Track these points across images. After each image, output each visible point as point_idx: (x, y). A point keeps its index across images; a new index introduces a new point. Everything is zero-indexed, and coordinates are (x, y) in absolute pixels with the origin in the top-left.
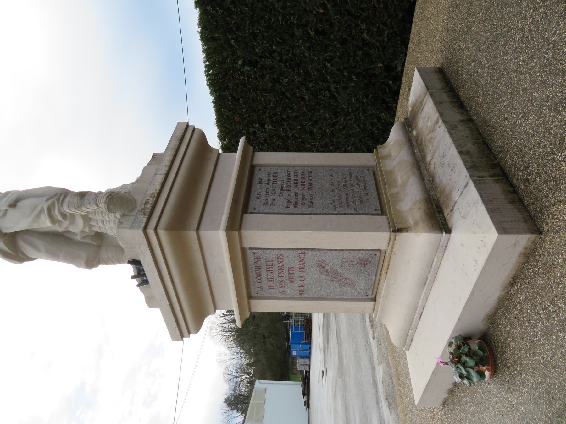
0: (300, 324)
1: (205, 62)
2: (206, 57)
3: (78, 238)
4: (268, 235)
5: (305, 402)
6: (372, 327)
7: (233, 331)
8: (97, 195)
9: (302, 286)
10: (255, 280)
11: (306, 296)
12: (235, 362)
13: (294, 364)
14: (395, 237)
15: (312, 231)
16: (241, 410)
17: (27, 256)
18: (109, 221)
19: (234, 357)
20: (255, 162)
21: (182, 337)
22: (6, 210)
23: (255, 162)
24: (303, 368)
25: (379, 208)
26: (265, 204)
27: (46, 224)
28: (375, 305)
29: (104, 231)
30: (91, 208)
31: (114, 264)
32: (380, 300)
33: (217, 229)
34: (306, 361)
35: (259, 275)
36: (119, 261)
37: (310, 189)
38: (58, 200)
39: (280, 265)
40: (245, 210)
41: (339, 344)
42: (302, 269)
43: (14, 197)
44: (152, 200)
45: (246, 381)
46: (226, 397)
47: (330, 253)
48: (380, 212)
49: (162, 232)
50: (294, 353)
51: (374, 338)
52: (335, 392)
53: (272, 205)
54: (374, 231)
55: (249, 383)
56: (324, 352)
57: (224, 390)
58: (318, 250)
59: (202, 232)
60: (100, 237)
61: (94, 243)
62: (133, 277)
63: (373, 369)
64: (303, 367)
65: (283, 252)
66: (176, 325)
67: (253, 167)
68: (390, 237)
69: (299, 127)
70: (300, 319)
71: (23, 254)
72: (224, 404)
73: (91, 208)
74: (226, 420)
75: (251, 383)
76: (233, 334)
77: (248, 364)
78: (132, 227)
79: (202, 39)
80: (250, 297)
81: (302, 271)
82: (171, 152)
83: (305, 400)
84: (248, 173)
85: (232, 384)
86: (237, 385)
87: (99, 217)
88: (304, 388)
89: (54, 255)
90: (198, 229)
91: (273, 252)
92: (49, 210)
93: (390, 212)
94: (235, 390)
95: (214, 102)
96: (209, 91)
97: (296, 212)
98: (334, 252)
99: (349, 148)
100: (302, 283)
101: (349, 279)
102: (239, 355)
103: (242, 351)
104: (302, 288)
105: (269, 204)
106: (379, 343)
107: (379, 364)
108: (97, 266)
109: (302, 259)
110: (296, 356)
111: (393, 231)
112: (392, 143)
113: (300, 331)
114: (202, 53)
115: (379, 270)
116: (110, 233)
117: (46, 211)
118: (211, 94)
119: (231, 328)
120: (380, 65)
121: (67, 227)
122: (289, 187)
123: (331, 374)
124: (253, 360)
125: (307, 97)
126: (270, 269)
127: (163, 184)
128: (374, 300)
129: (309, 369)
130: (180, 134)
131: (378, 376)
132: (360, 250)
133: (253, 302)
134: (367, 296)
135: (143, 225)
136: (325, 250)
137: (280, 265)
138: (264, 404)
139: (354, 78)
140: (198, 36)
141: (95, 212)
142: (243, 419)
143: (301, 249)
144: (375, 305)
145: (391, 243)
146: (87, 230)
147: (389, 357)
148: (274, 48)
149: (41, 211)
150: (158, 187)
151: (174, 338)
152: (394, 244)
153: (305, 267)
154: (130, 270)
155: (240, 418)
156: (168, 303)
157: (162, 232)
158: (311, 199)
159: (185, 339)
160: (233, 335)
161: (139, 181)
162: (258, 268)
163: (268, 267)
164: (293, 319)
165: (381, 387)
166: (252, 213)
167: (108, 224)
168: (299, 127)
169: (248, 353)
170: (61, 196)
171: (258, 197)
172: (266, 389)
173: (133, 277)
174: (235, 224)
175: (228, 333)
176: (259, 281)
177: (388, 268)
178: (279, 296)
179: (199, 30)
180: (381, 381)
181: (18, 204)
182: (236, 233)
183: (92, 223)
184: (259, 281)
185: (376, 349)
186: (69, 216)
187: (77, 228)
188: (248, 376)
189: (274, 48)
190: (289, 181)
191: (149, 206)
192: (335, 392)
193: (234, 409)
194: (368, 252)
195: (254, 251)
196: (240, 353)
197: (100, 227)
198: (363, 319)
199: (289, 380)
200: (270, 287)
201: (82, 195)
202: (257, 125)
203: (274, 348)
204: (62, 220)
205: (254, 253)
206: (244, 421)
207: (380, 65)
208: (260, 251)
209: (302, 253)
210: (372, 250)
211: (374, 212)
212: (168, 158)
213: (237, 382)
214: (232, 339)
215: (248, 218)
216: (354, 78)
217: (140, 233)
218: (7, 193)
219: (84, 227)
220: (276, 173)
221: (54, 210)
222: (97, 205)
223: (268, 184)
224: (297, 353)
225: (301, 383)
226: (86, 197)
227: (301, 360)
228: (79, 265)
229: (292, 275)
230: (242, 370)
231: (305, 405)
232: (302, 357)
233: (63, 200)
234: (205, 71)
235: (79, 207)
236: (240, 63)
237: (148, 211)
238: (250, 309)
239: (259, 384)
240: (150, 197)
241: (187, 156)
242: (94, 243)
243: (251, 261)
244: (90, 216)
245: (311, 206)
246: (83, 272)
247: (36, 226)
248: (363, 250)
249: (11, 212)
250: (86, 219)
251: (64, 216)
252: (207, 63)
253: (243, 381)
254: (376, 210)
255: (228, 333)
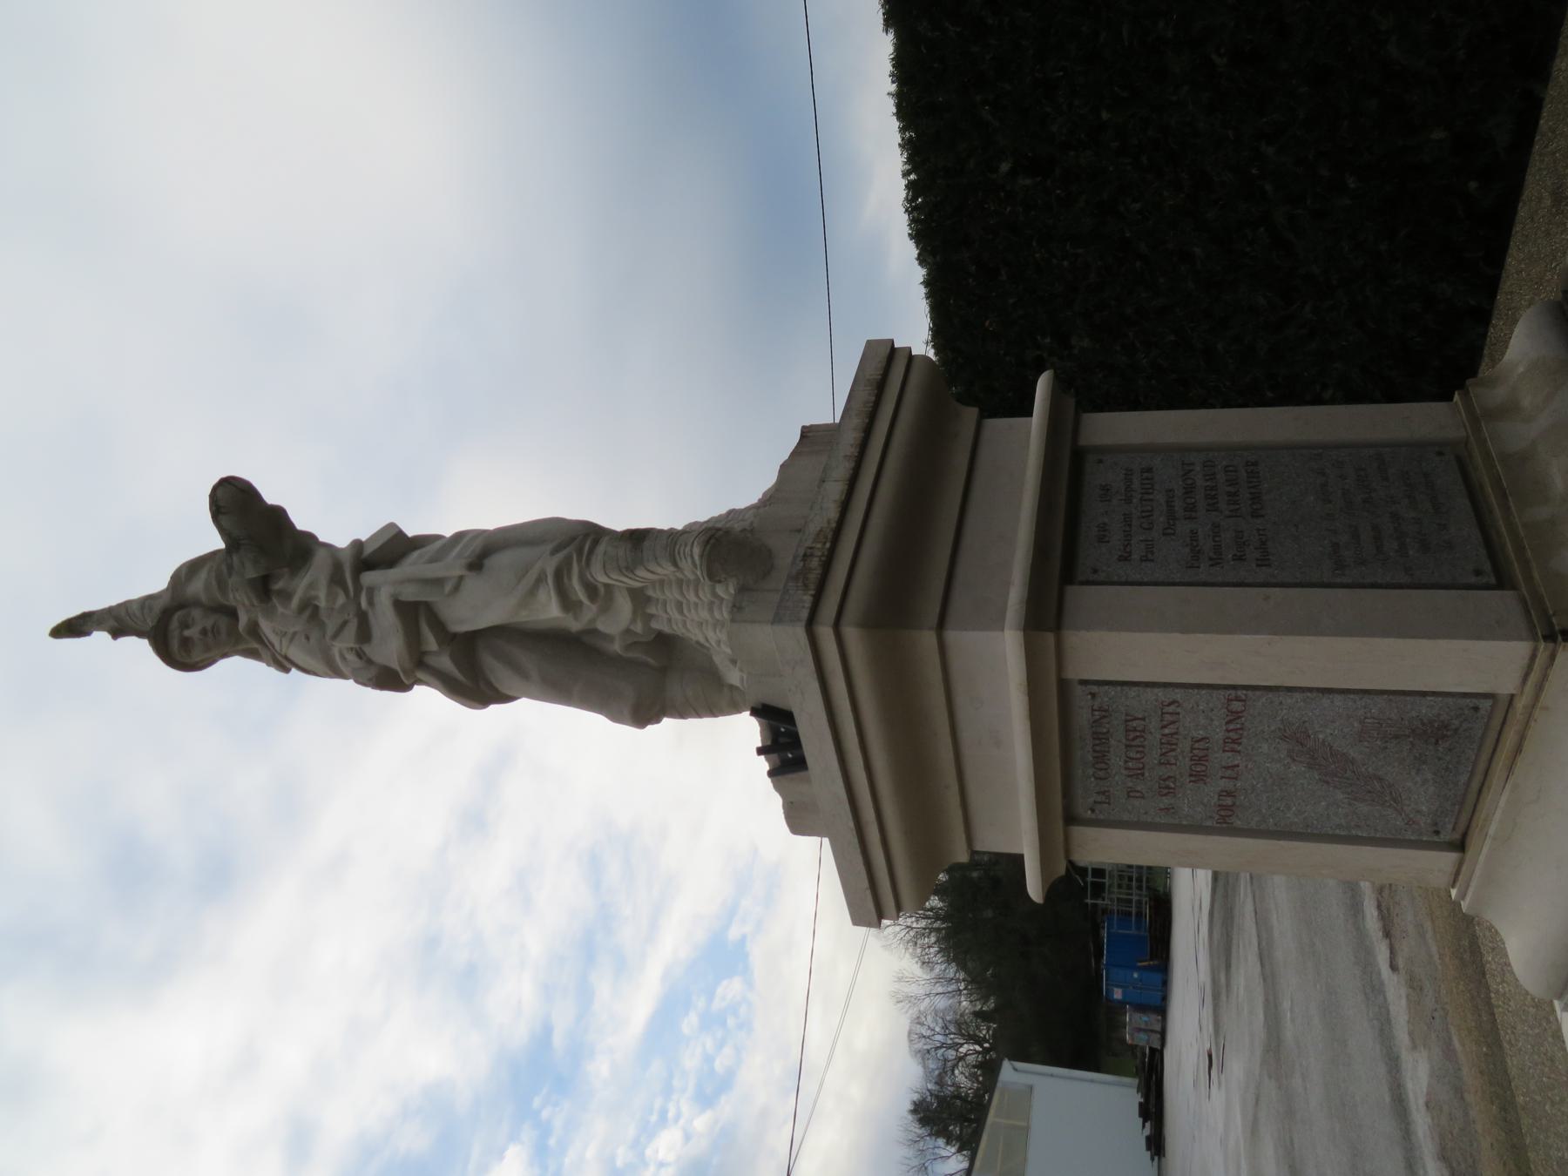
0: (1134, 911)
1: (905, 174)
2: (910, 160)
3: (616, 647)
4: (1143, 648)
5: (1148, 1138)
6: (1387, 934)
7: (937, 918)
8: (672, 536)
9: (1229, 794)
10: (1091, 771)
11: (1238, 823)
12: (942, 1003)
13: (1116, 1025)
14: (1553, 657)
15: (1275, 634)
16: (959, 1138)
17: (496, 690)
18: (696, 605)
19: (940, 990)
20: (1083, 442)
21: (881, 915)
22: (461, 578)
23: (1083, 441)
24: (1142, 1040)
25: (1487, 567)
26: (1125, 558)
27: (548, 611)
28: (1460, 864)
29: (678, 630)
30: (659, 570)
31: (699, 716)
32: (1482, 852)
33: (997, 624)
34: (1151, 1020)
35: (1101, 758)
36: (735, 708)
37: (1255, 514)
38: (580, 551)
39: (1166, 731)
40: (1069, 575)
41: (1269, 977)
42: (1232, 743)
43: (477, 545)
44: (821, 549)
45: (971, 1059)
46: (916, 1097)
47: (1325, 701)
48: (1493, 580)
49: (852, 634)
50: (1118, 994)
51: (1393, 967)
52: (1255, 1120)
53: (1145, 559)
54: (1479, 638)
55: (979, 1066)
56: (1216, 997)
57: (907, 1078)
58: (1290, 689)
59: (953, 636)
60: (665, 645)
61: (651, 661)
62: (760, 751)
63: (1393, 1063)
64: (1143, 1036)
65: (1178, 695)
66: (865, 883)
67: (1079, 455)
68: (1533, 657)
69: (1172, 338)
70: (1135, 898)
71: (490, 685)
72: (910, 1117)
73: (659, 570)
74: (915, 1162)
75: (988, 1070)
76: (938, 924)
77: (977, 1014)
78: (777, 619)
79: (901, 113)
80: (1071, 819)
81: (1233, 751)
82: (857, 421)
83: (1147, 1131)
84: (1068, 468)
85: (932, 1065)
86: (946, 1069)
87: (672, 594)
88: (1146, 1096)
89: (559, 690)
90: (941, 625)
91: (1150, 694)
92: (560, 576)
93: (1529, 578)
94: (940, 1082)
95: (927, 283)
96: (915, 252)
97: (1220, 579)
98: (1338, 699)
99: (1328, 394)
100: (1229, 785)
101: (1380, 779)
102: (953, 987)
103: (962, 975)
104: (1229, 801)
105: (1135, 556)
106: (1414, 984)
107: (1414, 1047)
108: (658, 721)
109: (1235, 716)
110: (1122, 1003)
111: (1545, 638)
112: (1521, 369)
113: (1133, 931)
114: (898, 151)
115: (1484, 757)
116: (695, 635)
117: (550, 580)
118: (922, 260)
119: (931, 909)
120: (1438, 135)
121: (593, 620)
122: (1191, 508)
123: (1238, 1067)
124: (991, 1004)
125: (1197, 250)
126: (1137, 742)
127: (845, 506)
128: (1460, 846)
129: (1163, 1043)
130: (874, 372)
131: (1409, 1085)
132: (1424, 694)
133: (1081, 833)
134: (1437, 833)
135: (805, 614)
136: (1310, 690)
137: (1166, 731)
138: (1027, 1129)
139: (1351, 183)
140: (890, 106)
141: (662, 582)
142: (965, 1165)
143: (1234, 687)
144: (1460, 864)
145: (1536, 676)
146: (638, 628)
147: (1453, 1030)
148: (1105, 115)
149: (540, 579)
150: (833, 513)
151: (858, 920)
152: (1545, 677)
153: (1244, 741)
154: (745, 729)
155: (956, 1162)
156: (851, 824)
157: (852, 634)
158: (1263, 543)
159: (885, 922)
160: (938, 930)
161: (769, 499)
162: (1101, 738)
163: (1132, 735)
164: (1114, 897)
165: (1422, 1123)
166: (1088, 583)
167: (699, 615)
168: (1172, 338)
169: (977, 983)
170: (583, 539)
171: (1102, 539)
172: (1031, 1088)
173: (760, 751)
174: (1045, 616)
175: (923, 923)
176: (1101, 774)
177: (1518, 750)
178: (1157, 820)
179: (893, 88)
180: (1421, 1101)
181: (488, 562)
182: (1050, 638)
183: (652, 610)
184: (1101, 774)
185: (1404, 1002)
186: (602, 590)
187: (617, 622)
188: (978, 1048)
189: (1105, 115)
190: (1189, 490)
191: (815, 563)
192: (1255, 1120)
193: (938, 1134)
194: (1450, 700)
195: (1095, 689)
196: (958, 981)
197: (669, 620)
198: (1355, 908)
199: (1097, 1068)
200: (1130, 793)
201: (637, 538)
202: (1048, 340)
203: (1045, 974)
204: (586, 601)
205: (1093, 695)
206: (969, 1172)
207: (1438, 135)
208: (1112, 691)
209: (1238, 699)
210: (1465, 695)
211: (1473, 580)
212: (851, 438)
213: (946, 1060)
214: (933, 939)
215: (1082, 597)
216: (1351, 183)
217: (800, 631)
218: (459, 536)
219: (633, 620)
220: (1149, 470)
221: (570, 579)
222: (675, 564)
223: (1128, 500)
224: (1124, 994)
225: (1136, 1081)
226: (646, 544)
227: (1137, 1016)
228: (616, 718)
229: (1201, 759)
230: (962, 1028)
231: (1149, 1148)
232: (1141, 1008)
233: (591, 551)
234: (906, 199)
235: (630, 569)
236: (1005, 167)
237: (814, 576)
238: (1067, 852)
239: (1011, 1073)
240: (815, 541)
241: (907, 430)
242: (651, 661)
243: (1083, 718)
244: (650, 593)
245: (1263, 562)
246: (626, 731)
247: (525, 617)
248: (1434, 694)
249: (473, 583)
250: (639, 598)
251: (592, 590)
252: (912, 177)
253: (961, 1059)
254: (1478, 573)
255: (923, 923)
